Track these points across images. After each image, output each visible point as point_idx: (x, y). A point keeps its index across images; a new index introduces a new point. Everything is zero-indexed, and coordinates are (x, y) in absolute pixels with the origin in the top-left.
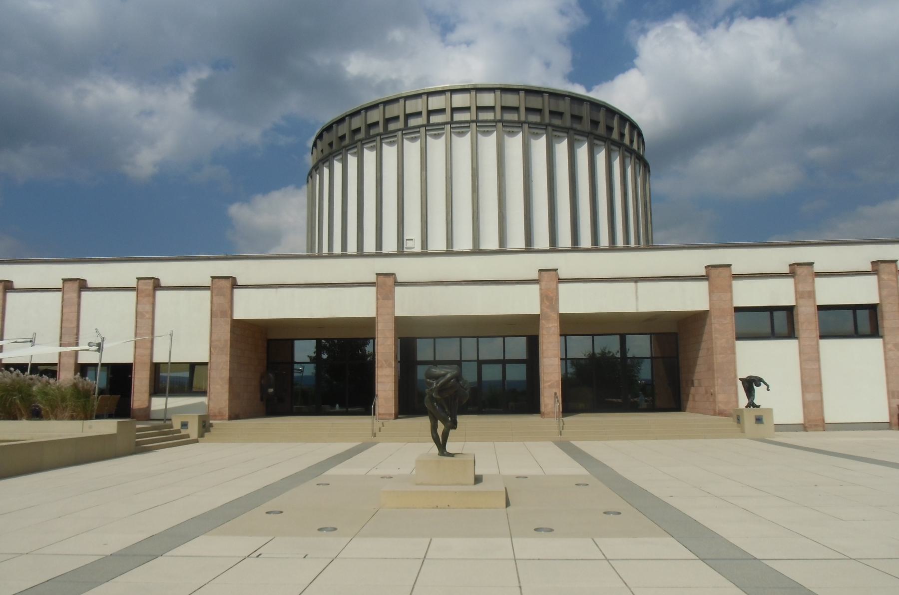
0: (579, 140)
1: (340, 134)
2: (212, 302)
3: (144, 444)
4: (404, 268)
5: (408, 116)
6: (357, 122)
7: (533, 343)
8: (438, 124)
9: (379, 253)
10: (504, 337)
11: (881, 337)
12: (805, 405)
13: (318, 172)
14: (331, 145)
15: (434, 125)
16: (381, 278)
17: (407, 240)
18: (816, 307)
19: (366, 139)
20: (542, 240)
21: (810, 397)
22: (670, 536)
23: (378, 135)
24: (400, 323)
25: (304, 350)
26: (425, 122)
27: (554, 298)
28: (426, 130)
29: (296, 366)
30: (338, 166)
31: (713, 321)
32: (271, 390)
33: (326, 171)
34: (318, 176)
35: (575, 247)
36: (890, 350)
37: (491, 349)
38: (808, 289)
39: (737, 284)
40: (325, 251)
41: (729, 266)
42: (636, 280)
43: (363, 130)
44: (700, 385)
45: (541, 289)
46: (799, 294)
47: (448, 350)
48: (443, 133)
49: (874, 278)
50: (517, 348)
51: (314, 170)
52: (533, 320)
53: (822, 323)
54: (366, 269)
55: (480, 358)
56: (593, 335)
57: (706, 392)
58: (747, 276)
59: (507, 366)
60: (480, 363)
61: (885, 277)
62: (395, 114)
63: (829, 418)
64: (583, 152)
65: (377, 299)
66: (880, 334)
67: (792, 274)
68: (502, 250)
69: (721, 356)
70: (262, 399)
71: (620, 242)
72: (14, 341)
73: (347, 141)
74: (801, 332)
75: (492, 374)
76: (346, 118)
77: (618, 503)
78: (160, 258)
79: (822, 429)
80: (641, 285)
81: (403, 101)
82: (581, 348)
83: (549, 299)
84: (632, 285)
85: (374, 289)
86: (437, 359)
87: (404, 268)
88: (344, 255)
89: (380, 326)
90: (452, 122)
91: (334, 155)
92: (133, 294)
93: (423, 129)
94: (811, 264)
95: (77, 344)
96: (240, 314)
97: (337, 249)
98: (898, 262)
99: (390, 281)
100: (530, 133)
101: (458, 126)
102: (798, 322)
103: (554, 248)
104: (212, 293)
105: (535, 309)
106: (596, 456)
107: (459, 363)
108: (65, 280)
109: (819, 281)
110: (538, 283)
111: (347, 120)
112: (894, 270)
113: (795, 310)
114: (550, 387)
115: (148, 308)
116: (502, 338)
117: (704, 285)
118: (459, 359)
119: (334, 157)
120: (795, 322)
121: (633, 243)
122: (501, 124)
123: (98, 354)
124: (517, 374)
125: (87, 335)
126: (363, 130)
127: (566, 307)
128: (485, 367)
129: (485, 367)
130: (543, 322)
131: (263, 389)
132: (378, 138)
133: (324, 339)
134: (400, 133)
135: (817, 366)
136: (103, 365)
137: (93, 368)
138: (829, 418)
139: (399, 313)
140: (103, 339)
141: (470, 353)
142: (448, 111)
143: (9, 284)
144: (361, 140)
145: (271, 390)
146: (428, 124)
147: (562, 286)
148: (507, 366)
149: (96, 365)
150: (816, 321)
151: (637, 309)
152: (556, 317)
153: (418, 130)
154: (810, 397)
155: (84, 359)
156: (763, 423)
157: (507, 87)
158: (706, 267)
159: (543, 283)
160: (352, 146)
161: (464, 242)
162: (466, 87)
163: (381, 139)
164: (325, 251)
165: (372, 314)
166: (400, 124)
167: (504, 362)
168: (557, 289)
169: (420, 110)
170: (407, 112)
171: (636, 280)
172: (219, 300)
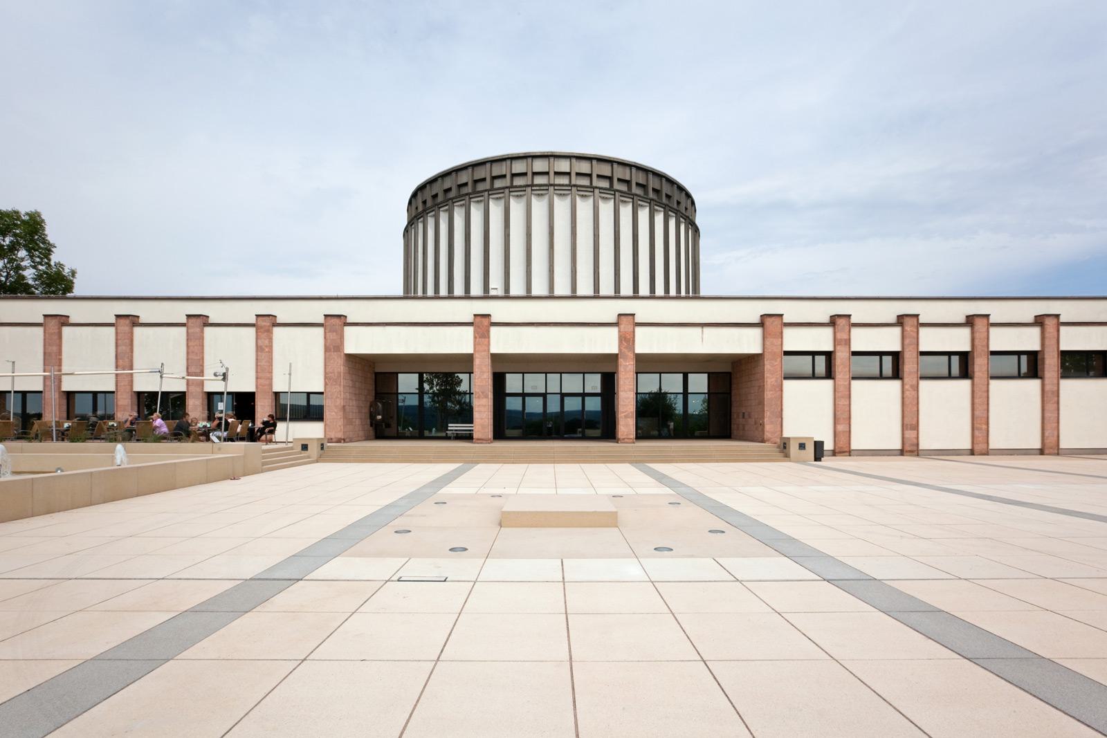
0: (642, 206)
1: (434, 193)
2: (325, 338)
4: (499, 311)
5: (494, 178)
6: (448, 183)
7: (609, 381)
8: (520, 186)
9: (617, 296)
10: (660, 373)
11: (833, 379)
13: (413, 226)
14: (435, 196)
15: (516, 187)
16: (479, 319)
17: (492, 289)
19: (456, 197)
20: (626, 289)
22: (781, 555)
23: (467, 194)
24: (496, 358)
25: (408, 383)
26: (508, 184)
29: (400, 397)
30: (431, 222)
31: (765, 362)
32: (379, 417)
33: (421, 226)
34: (413, 230)
35: (652, 296)
36: (908, 390)
37: (572, 383)
38: (845, 337)
39: (788, 332)
40: (420, 293)
41: (782, 315)
43: (470, 184)
44: (750, 417)
45: (619, 331)
46: (836, 341)
47: (535, 383)
48: (524, 195)
49: (897, 330)
50: (594, 383)
51: (409, 226)
52: (613, 358)
53: (1063, 365)
54: (465, 310)
55: (563, 392)
56: (584, 373)
57: (756, 423)
59: (586, 398)
60: (563, 396)
61: (908, 328)
62: (483, 177)
64: (644, 214)
65: (475, 338)
66: (900, 376)
67: (761, 324)
70: (371, 425)
71: (673, 292)
72: (149, 371)
74: (837, 373)
75: (572, 405)
77: (721, 525)
79: (848, 454)
80: (706, 330)
82: (650, 384)
83: (627, 340)
84: (698, 330)
85: (471, 329)
86: (586, 391)
87: (499, 311)
88: (437, 297)
89: (477, 362)
90: (512, 186)
91: (427, 211)
92: (252, 330)
93: (507, 191)
94: (849, 316)
95: (203, 376)
96: (350, 348)
97: (430, 292)
98: (852, 317)
99: (485, 322)
100: (600, 197)
101: (542, 188)
102: (835, 365)
103: (486, 296)
104: (325, 329)
105: (613, 349)
106: (675, 477)
107: (544, 396)
108: (620, 315)
109: (854, 331)
112: (916, 324)
113: (900, 354)
115: (55, 348)
117: (757, 332)
118: (544, 392)
119: (428, 213)
121: (683, 293)
123: (223, 383)
124: (594, 405)
125: (211, 366)
126: (470, 184)
127: (640, 349)
128: (567, 400)
129: (567, 400)
130: (621, 361)
131: (372, 417)
132: (467, 197)
133: (425, 373)
134: (486, 193)
136: (229, 393)
137: (219, 396)
139: (494, 350)
140: (227, 369)
141: (553, 387)
142: (508, 176)
143: (136, 319)
144: (452, 199)
145: (379, 417)
146: (492, 189)
147: (638, 330)
148: (586, 398)
149: (222, 393)
152: (631, 355)
153: (524, 189)
154: (840, 428)
155: (210, 387)
157: (581, 155)
159: (622, 326)
160: (458, 199)
161: (562, 288)
162: (546, 154)
163: (470, 198)
164: (420, 293)
165: (470, 351)
166: (487, 185)
167: (584, 395)
169: (504, 173)
170: (493, 175)
172: (332, 336)
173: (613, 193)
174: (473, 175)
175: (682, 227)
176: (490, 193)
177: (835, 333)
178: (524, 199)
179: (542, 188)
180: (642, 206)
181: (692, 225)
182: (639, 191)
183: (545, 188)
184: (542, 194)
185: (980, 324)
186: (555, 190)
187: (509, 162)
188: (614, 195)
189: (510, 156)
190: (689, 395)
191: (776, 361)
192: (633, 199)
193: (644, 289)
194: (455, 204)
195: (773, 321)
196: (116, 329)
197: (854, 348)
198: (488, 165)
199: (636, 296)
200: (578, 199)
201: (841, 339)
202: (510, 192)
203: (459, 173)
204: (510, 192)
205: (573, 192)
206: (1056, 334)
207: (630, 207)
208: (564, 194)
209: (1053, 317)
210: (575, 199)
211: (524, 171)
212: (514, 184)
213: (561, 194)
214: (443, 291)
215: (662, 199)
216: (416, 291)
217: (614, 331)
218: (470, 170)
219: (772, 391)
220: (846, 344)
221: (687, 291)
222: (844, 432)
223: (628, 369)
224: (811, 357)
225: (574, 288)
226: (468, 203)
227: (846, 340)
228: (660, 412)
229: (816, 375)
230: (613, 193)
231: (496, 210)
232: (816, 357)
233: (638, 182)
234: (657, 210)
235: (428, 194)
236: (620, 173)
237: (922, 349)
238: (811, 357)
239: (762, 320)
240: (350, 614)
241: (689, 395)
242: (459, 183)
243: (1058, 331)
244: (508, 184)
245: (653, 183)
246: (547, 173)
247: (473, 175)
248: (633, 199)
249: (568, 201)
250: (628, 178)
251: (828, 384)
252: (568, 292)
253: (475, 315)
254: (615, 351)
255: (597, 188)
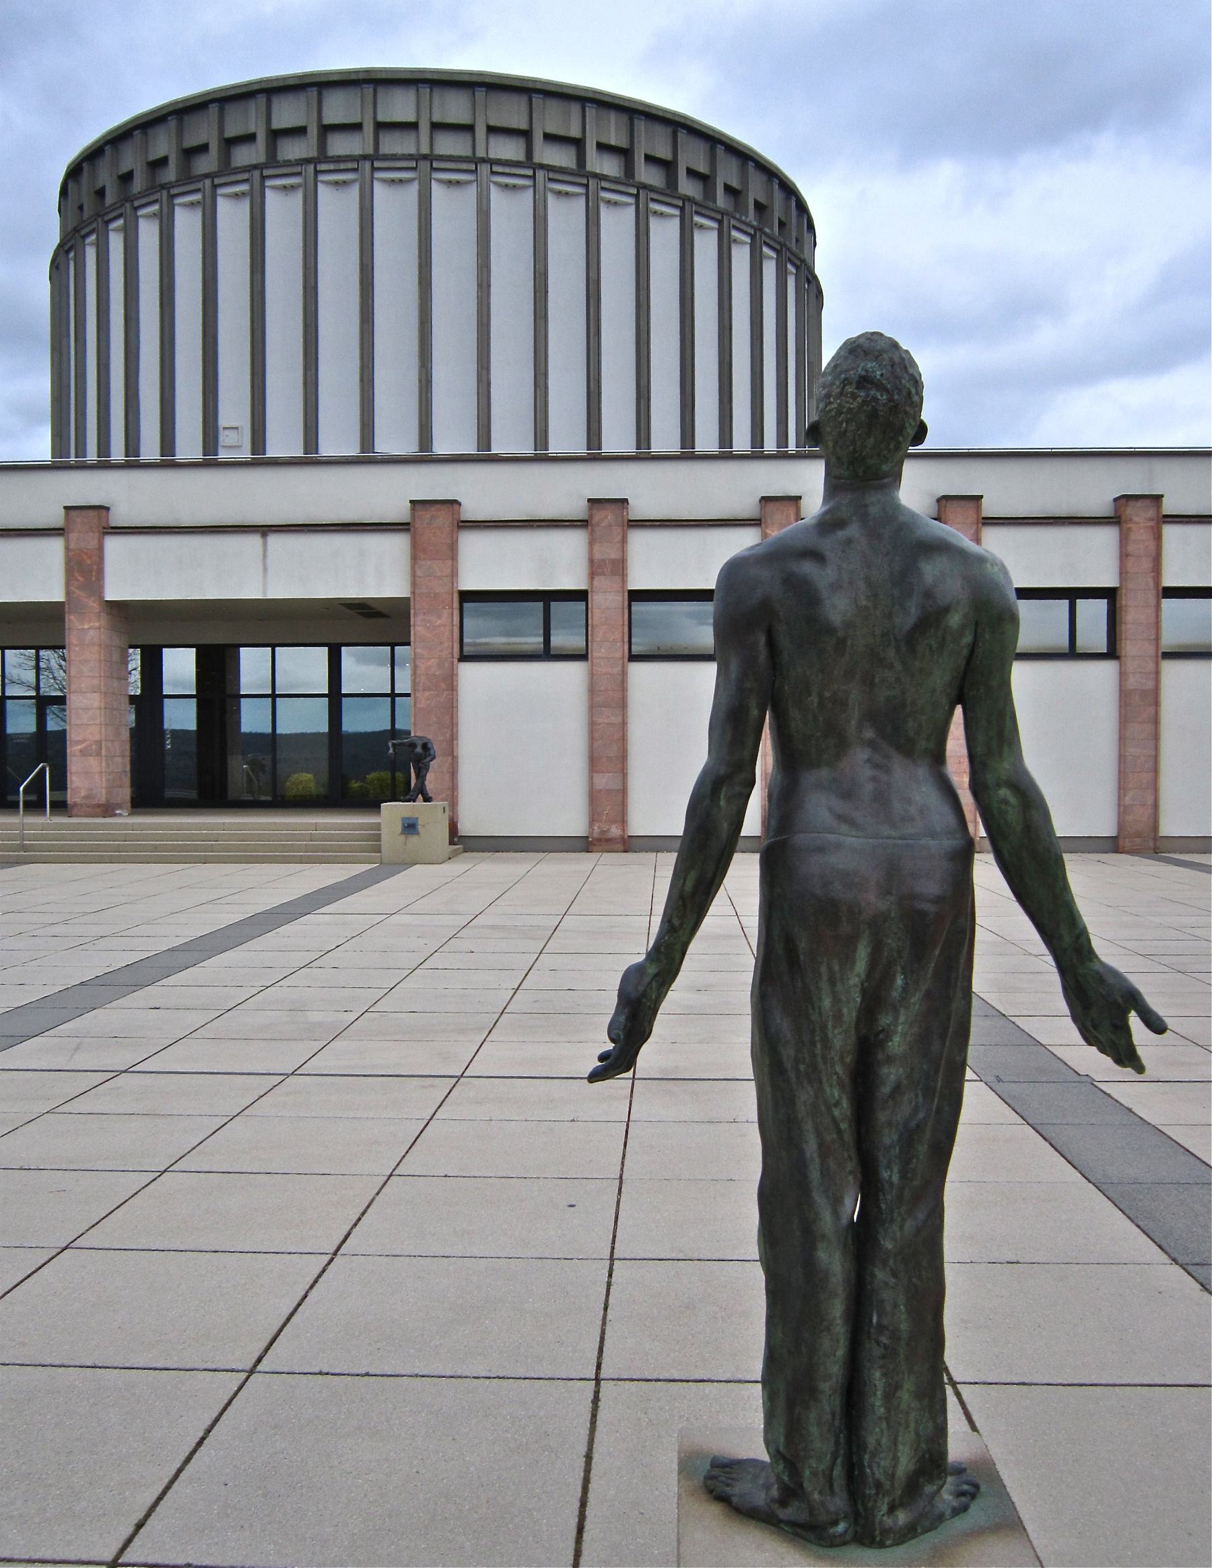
0: (662, 214)
3: (1165, 853)
9: (594, 455)
12: (594, 797)
15: (386, 158)
17: (225, 428)
18: (626, 594)
19: (142, 195)
21: (604, 781)
23: (206, 176)
27: (95, 567)
28: (317, 172)
35: (688, 453)
38: (614, 554)
40: (92, 456)
42: (265, 530)
45: (67, 548)
46: (595, 568)
58: (471, 526)
63: (1170, 827)
68: (310, 459)
69: (427, 693)
71: (770, 445)
73: (170, 174)
76: (107, 148)
78: (425, 458)
79: (620, 847)
81: (315, 93)
91: (83, 232)
98: (1164, 499)
99: (443, 518)
101: (342, 166)
106: (718, 907)
108: (765, 500)
110: (408, 530)
111: (106, 152)
114: (84, 753)
116: (389, 648)
120: (1117, 622)
122: (428, 163)
130: (72, 620)
135: (620, 719)
138: (1170, 827)
142: (313, 132)
146: (323, 156)
150: (69, 629)
151: (265, 595)
154: (604, 781)
156: (418, 833)
158: (1116, 500)
159: (73, 536)
162: (353, 77)
168: (101, 549)
171: (265, 530)
173: (530, 173)
174: (221, 129)
175: (769, 270)
176: (217, 181)
177: (591, 543)
178: (471, 193)
179: (342, 166)
180: (662, 214)
181: (797, 267)
182: (609, 166)
183: (350, 165)
184: (458, 183)
185: (1140, 517)
186: (493, 173)
187: (262, 99)
188: (534, 177)
189: (264, 86)
190: (344, 699)
191: (440, 617)
192: (587, 186)
193: (665, 437)
194: (141, 212)
195: (433, 517)
196: (1124, 541)
197: (638, 581)
198: (214, 109)
199: (643, 454)
200: (495, 194)
201: (603, 561)
202: (374, 169)
203: (151, 131)
204: (374, 169)
205: (363, 176)
206: (1151, 545)
207: (628, 216)
208: (401, 181)
209: (1147, 502)
210: (545, 201)
211: (355, 119)
212: (280, 157)
213: (393, 181)
214: (150, 449)
215: (715, 201)
216: (81, 450)
217: (54, 548)
218: (173, 123)
219: (429, 689)
220: (614, 573)
221: (726, 434)
222: (609, 791)
223: (88, 638)
224: (1066, 603)
225: (541, 434)
226: (208, 202)
227: (614, 562)
228: (104, 758)
229: (1079, 651)
230: (530, 173)
231: (187, 224)
232: (1081, 604)
233: (603, 140)
234: (701, 227)
235: (105, 176)
236: (552, 119)
237: (1169, 581)
238: (1066, 603)
239: (1116, 510)
240: (59, 1250)
241: (344, 699)
242: (151, 158)
243: (1158, 537)
244: (313, 153)
245: (693, 156)
246: (413, 126)
247: (221, 129)
248: (587, 186)
249: (526, 200)
250: (575, 132)
251: (1107, 669)
252: (297, 450)
253: (66, 508)
254: (56, 594)
255: (542, 166)
